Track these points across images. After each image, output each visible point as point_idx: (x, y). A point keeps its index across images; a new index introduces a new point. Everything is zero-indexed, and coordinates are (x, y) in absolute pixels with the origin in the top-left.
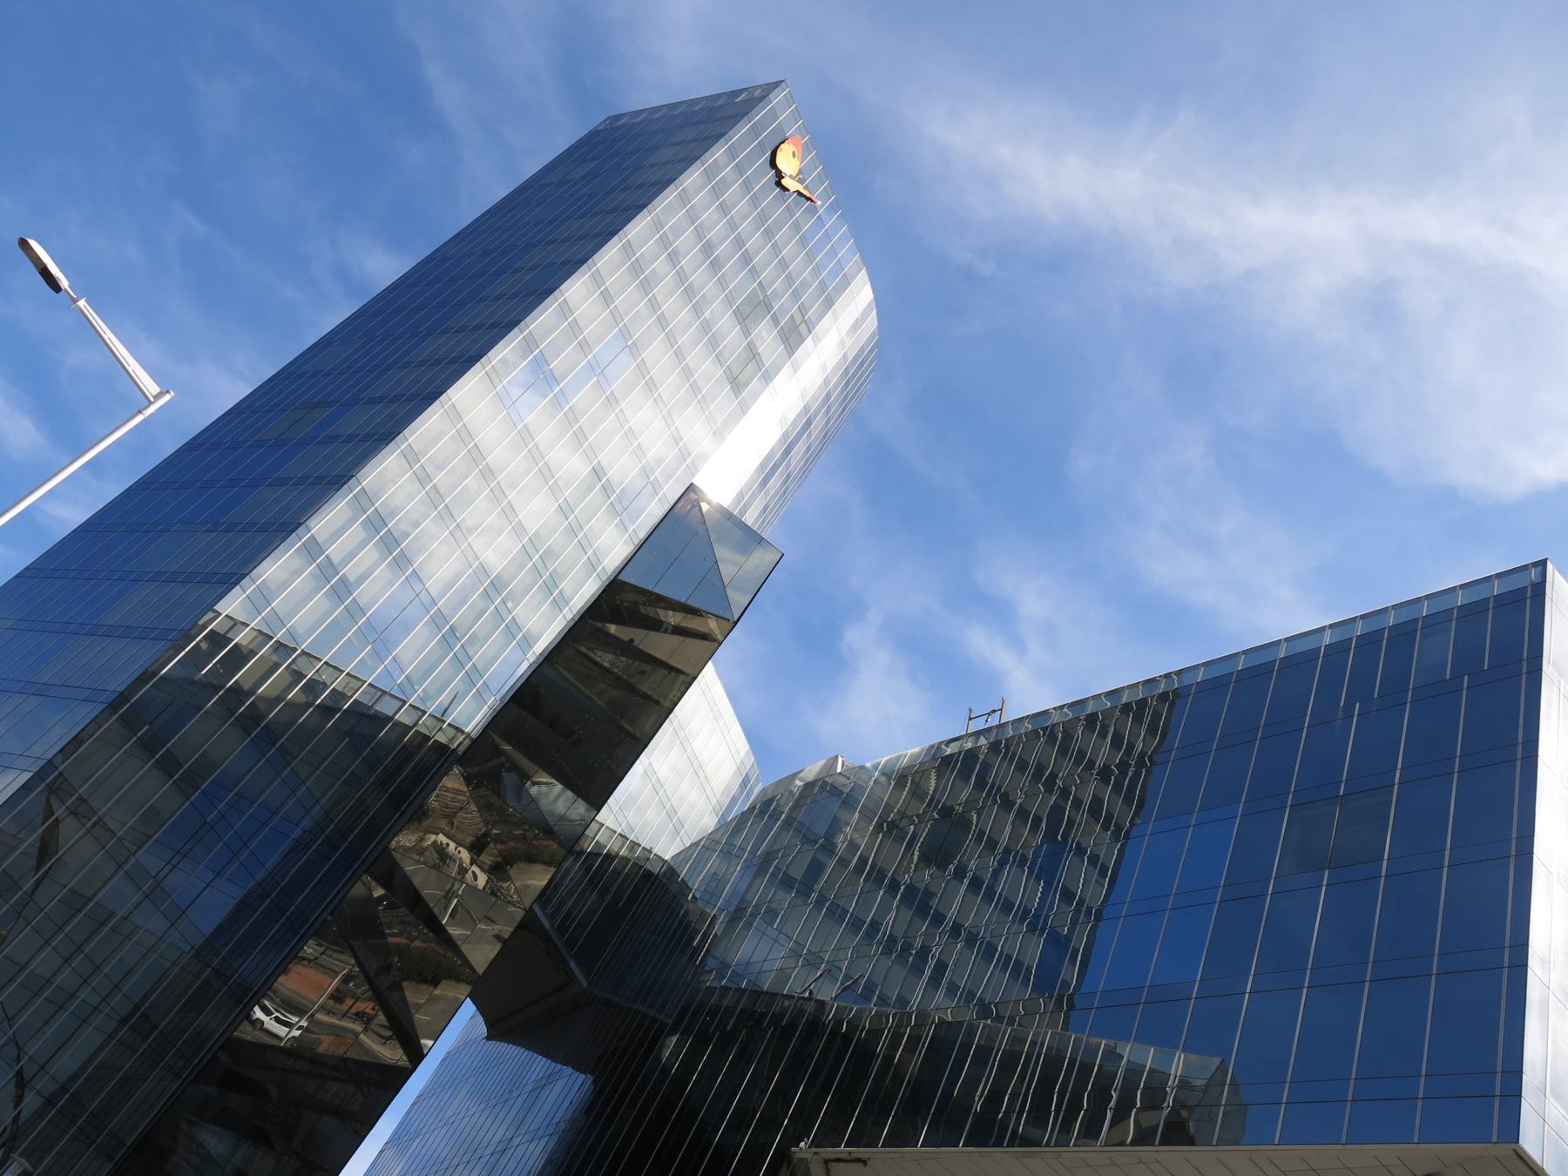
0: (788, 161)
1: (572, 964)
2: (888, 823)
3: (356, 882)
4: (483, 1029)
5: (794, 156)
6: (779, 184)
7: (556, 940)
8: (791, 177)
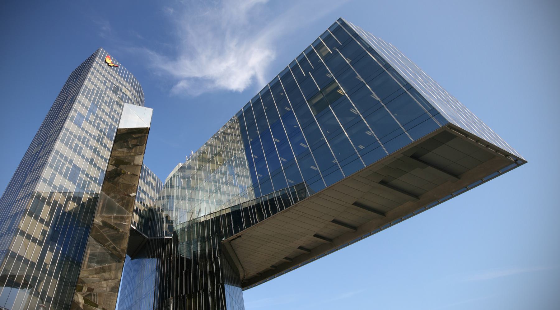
0: (109, 61)
1: (143, 234)
4: (130, 259)
6: (109, 66)
7: (138, 230)
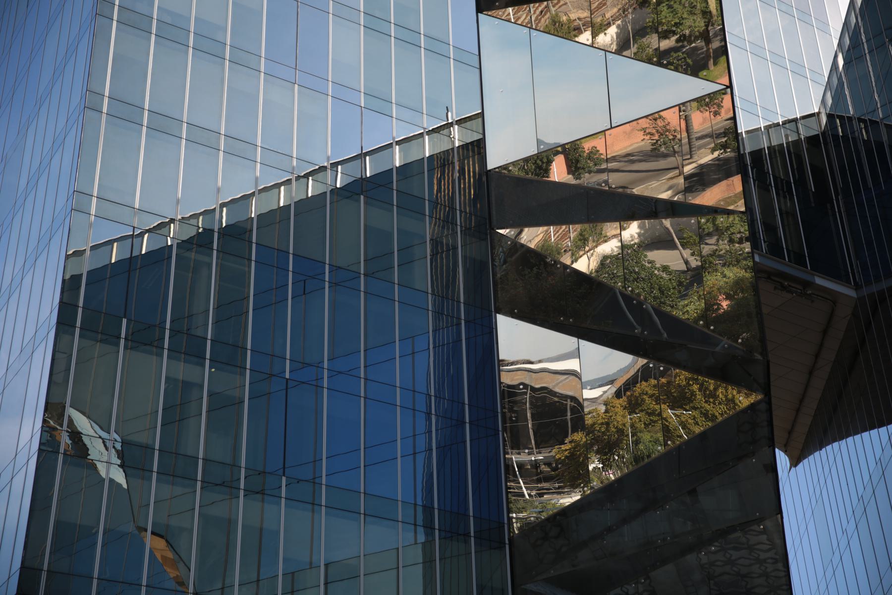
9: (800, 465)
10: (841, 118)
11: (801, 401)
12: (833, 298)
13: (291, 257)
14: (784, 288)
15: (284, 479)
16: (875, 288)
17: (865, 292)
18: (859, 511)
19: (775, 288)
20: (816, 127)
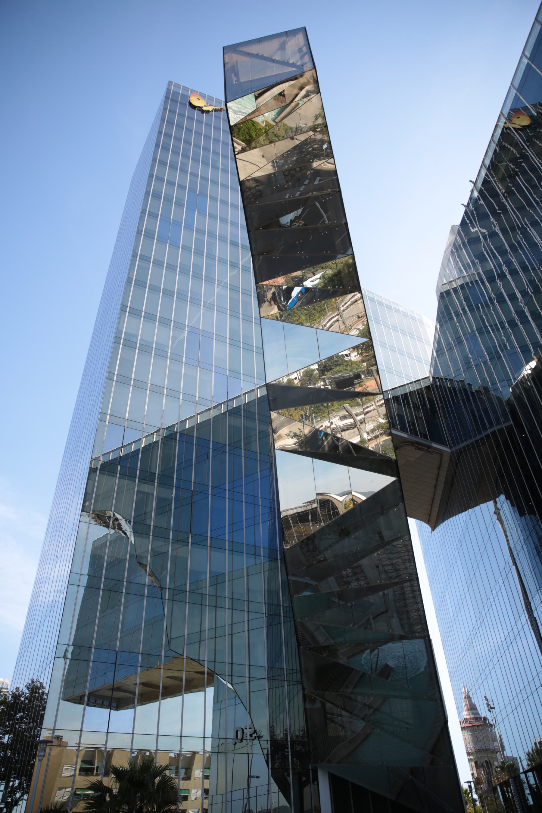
2: (509, 183)
3: (274, 451)
5: (199, 99)
8: (205, 106)
9: (436, 530)
10: (438, 378)
11: (433, 501)
12: (441, 453)
13: (211, 442)
14: (419, 449)
15: (190, 534)
16: (457, 447)
17: (454, 449)
18: (459, 546)
19: (416, 449)
20: (429, 382)
